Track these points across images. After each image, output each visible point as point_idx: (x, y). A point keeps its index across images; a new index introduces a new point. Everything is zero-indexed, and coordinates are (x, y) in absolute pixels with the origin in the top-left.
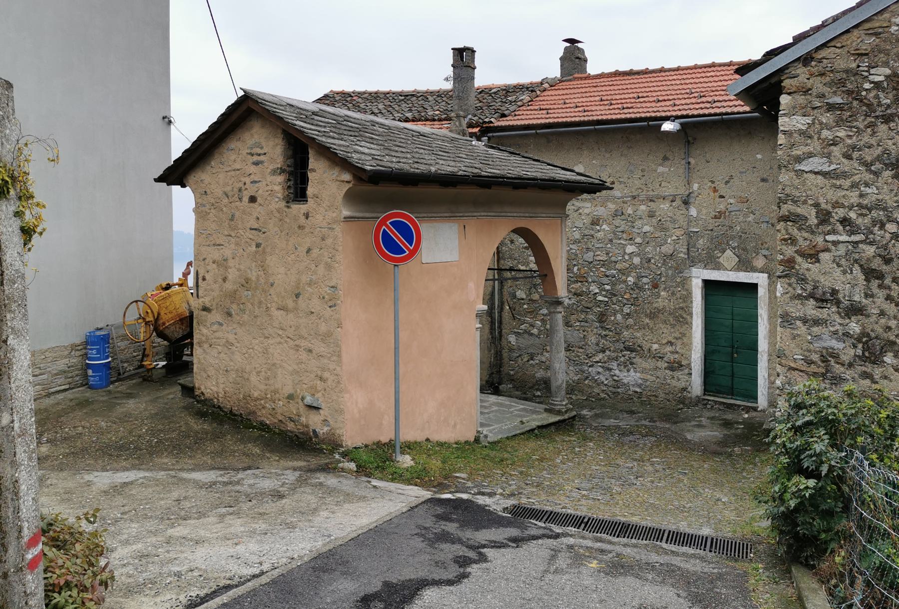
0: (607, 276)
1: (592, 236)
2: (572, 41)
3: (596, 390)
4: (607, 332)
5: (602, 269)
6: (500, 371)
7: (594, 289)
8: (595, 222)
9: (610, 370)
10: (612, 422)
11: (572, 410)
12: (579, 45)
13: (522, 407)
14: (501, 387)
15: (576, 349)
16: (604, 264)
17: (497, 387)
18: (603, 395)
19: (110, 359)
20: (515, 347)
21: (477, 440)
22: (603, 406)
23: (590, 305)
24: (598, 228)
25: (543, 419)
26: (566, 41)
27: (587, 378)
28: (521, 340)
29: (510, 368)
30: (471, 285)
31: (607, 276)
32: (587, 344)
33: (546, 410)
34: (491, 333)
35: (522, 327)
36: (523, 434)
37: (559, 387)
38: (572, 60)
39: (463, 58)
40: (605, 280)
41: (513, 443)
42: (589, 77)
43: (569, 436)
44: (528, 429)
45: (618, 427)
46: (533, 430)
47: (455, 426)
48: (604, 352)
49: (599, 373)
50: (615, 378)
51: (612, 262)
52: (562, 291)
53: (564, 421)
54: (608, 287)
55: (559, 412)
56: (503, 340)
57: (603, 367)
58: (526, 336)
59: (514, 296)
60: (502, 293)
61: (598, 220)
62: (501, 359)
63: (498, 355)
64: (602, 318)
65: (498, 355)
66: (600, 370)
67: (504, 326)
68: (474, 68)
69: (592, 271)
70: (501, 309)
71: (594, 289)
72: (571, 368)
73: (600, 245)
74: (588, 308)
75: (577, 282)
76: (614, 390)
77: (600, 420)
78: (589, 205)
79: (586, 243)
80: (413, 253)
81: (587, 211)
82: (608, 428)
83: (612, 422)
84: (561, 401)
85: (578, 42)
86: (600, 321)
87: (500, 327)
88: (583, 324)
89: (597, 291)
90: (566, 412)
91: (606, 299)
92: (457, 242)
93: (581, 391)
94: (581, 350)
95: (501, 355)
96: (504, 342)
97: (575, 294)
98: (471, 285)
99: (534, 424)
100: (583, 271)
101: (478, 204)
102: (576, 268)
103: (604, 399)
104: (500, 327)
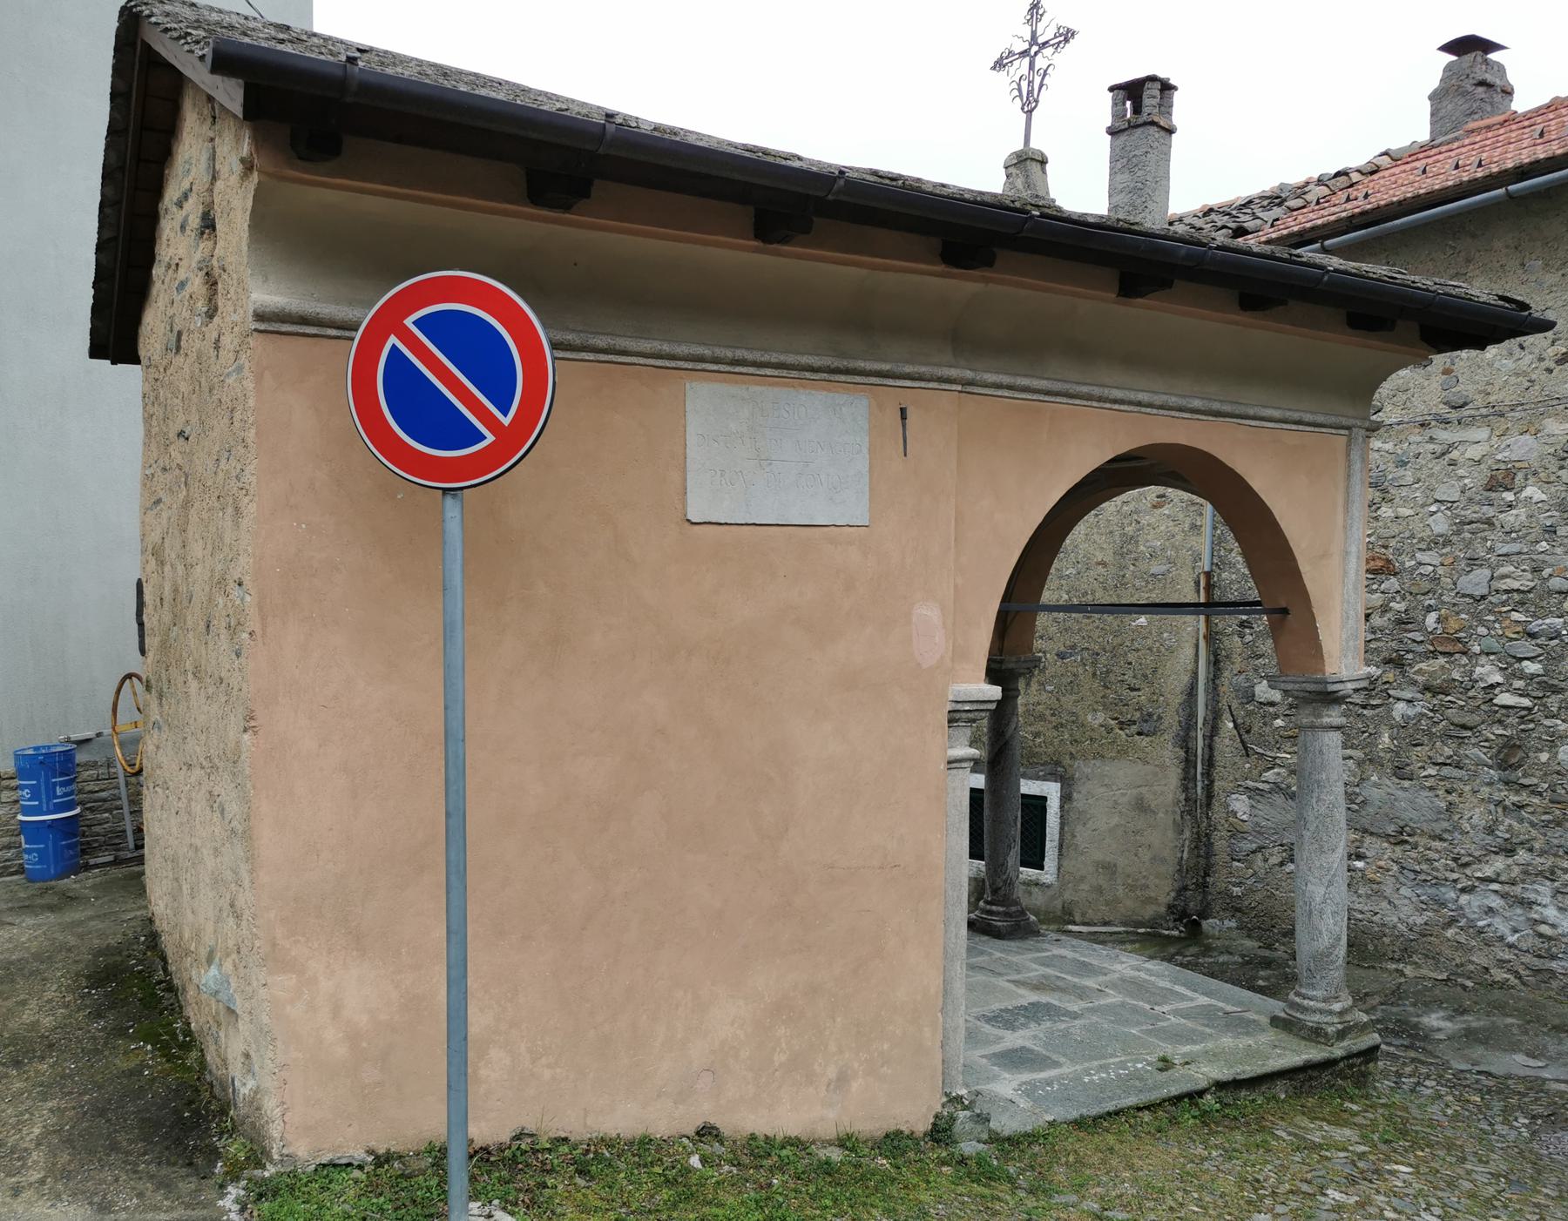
0: (1532, 636)
1: (1489, 522)
2: (1468, 47)
3: (1479, 959)
4: (1523, 797)
5: (1515, 616)
6: (1205, 885)
7: (1489, 672)
8: (1501, 480)
9: (1529, 904)
10: (1518, 1063)
11: (1363, 1028)
12: (1493, 56)
13: (1203, 1000)
14: (1206, 924)
15: (1423, 841)
16: (1522, 599)
17: (1197, 924)
18: (1499, 975)
19: (78, 811)
20: (1247, 827)
21: (941, 1132)
22: (1501, 1008)
23: (1468, 719)
24: (1509, 496)
25: (1250, 1053)
26: (1449, 48)
27: (1452, 922)
28: (1264, 809)
29: (1229, 878)
30: (928, 613)
31: (1532, 636)
32: (1456, 827)
33: (1275, 1021)
34: (1186, 789)
35: (1269, 775)
36: (1150, 1107)
37: (1322, 958)
38: (1464, 94)
39: (1142, 106)
40: (1526, 647)
41: (1087, 1146)
42: (1514, 118)
43: (1338, 1120)
44: (1175, 1090)
45: (1536, 1085)
46: (1194, 1096)
47: (842, 1080)
48: (1510, 852)
49: (1490, 911)
50: (1544, 929)
51: (1550, 593)
52: (1344, 658)
53: (1329, 1064)
54: (1532, 668)
55: (1316, 1035)
56: (1216, 804)
57: (1504, 896)
58: (1279, 799)
59: (1251, 697)
60: (1215, 688)
61: (1511, 474)
62: (1209, 854)
63: (1202, 843)
64: (1508, 757)
65: (1202, 843)
66: (1496, 902)
67: (1218, 772)
68: (1170, 131)
69: (1482, 623)
70: (1214, 730)
71: (1489, 672)
72: (1403, 891)
73: (1515, 547)
74: (1464, 727)
75: (1434, 654)
76: (1538, 963)
77: (1478, 1051)
78: (1481, 433)
79: (1468, 544)
80: (511, 441)
81: (1474, 452)
82: (1501, 1086)
83: (1518, 1063)
84: (1327, 998)
85: (1496, 47)
86: (1504, 765)
87: (1208, 774)
88: (1446, 771)
89: (1497, 678)
90: (1341, 1035)
91: (1526, 702)
92: (862, 464)
93: (1434, 957)
94: (1437, 844)
95: (1209, 845)
96: (1217, 813)
97: (1427, 688)
98: (928, 613)
99: (1207, 1073)
100: (1453, 625)
101: (966, 341)
102: (1431, 619)
103: (1503, 985)
104: (1208, 774)
